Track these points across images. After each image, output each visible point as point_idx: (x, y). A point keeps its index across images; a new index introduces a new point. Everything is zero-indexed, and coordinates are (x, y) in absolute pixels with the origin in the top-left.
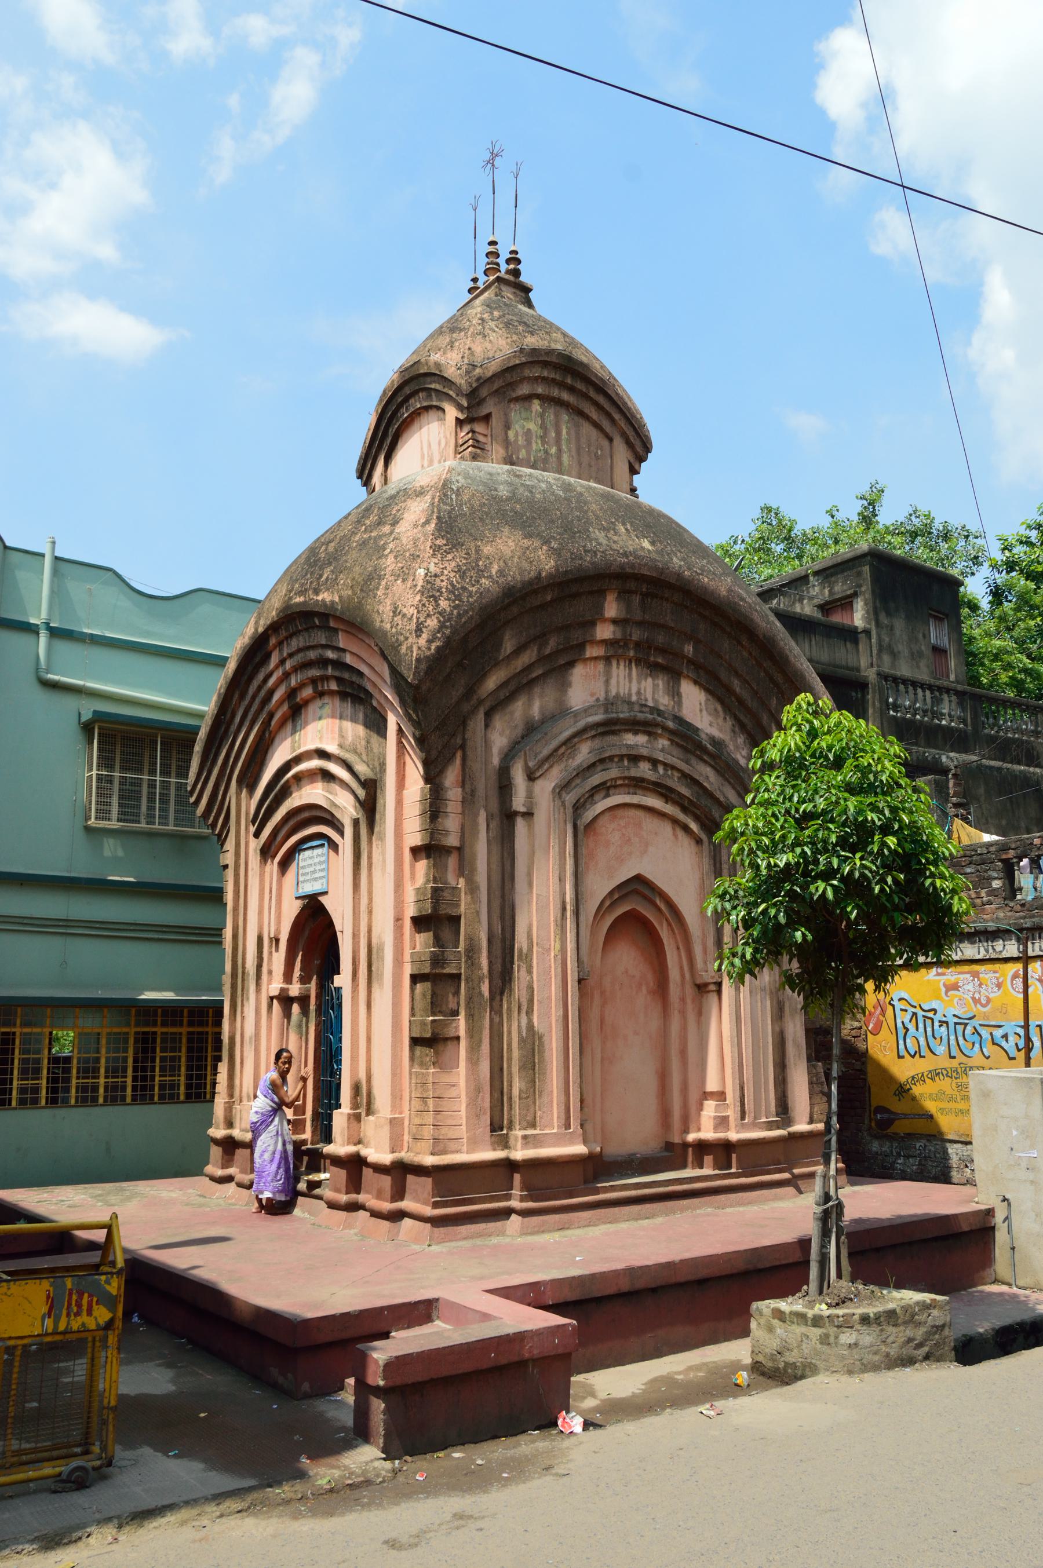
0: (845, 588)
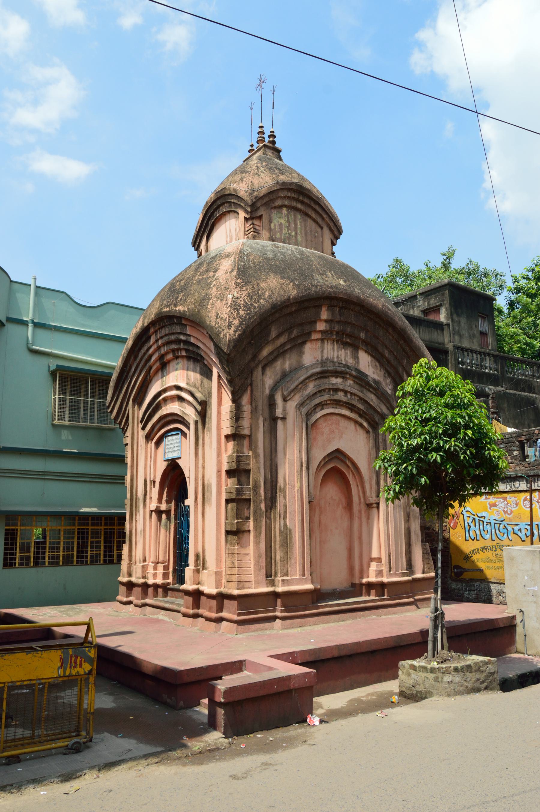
0: (436, 302)
